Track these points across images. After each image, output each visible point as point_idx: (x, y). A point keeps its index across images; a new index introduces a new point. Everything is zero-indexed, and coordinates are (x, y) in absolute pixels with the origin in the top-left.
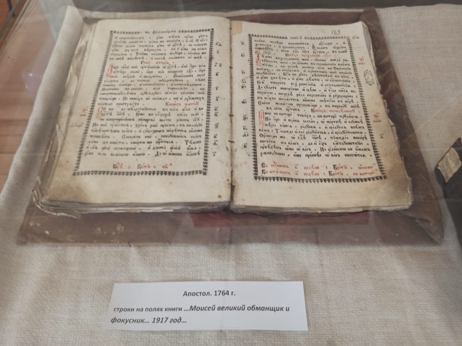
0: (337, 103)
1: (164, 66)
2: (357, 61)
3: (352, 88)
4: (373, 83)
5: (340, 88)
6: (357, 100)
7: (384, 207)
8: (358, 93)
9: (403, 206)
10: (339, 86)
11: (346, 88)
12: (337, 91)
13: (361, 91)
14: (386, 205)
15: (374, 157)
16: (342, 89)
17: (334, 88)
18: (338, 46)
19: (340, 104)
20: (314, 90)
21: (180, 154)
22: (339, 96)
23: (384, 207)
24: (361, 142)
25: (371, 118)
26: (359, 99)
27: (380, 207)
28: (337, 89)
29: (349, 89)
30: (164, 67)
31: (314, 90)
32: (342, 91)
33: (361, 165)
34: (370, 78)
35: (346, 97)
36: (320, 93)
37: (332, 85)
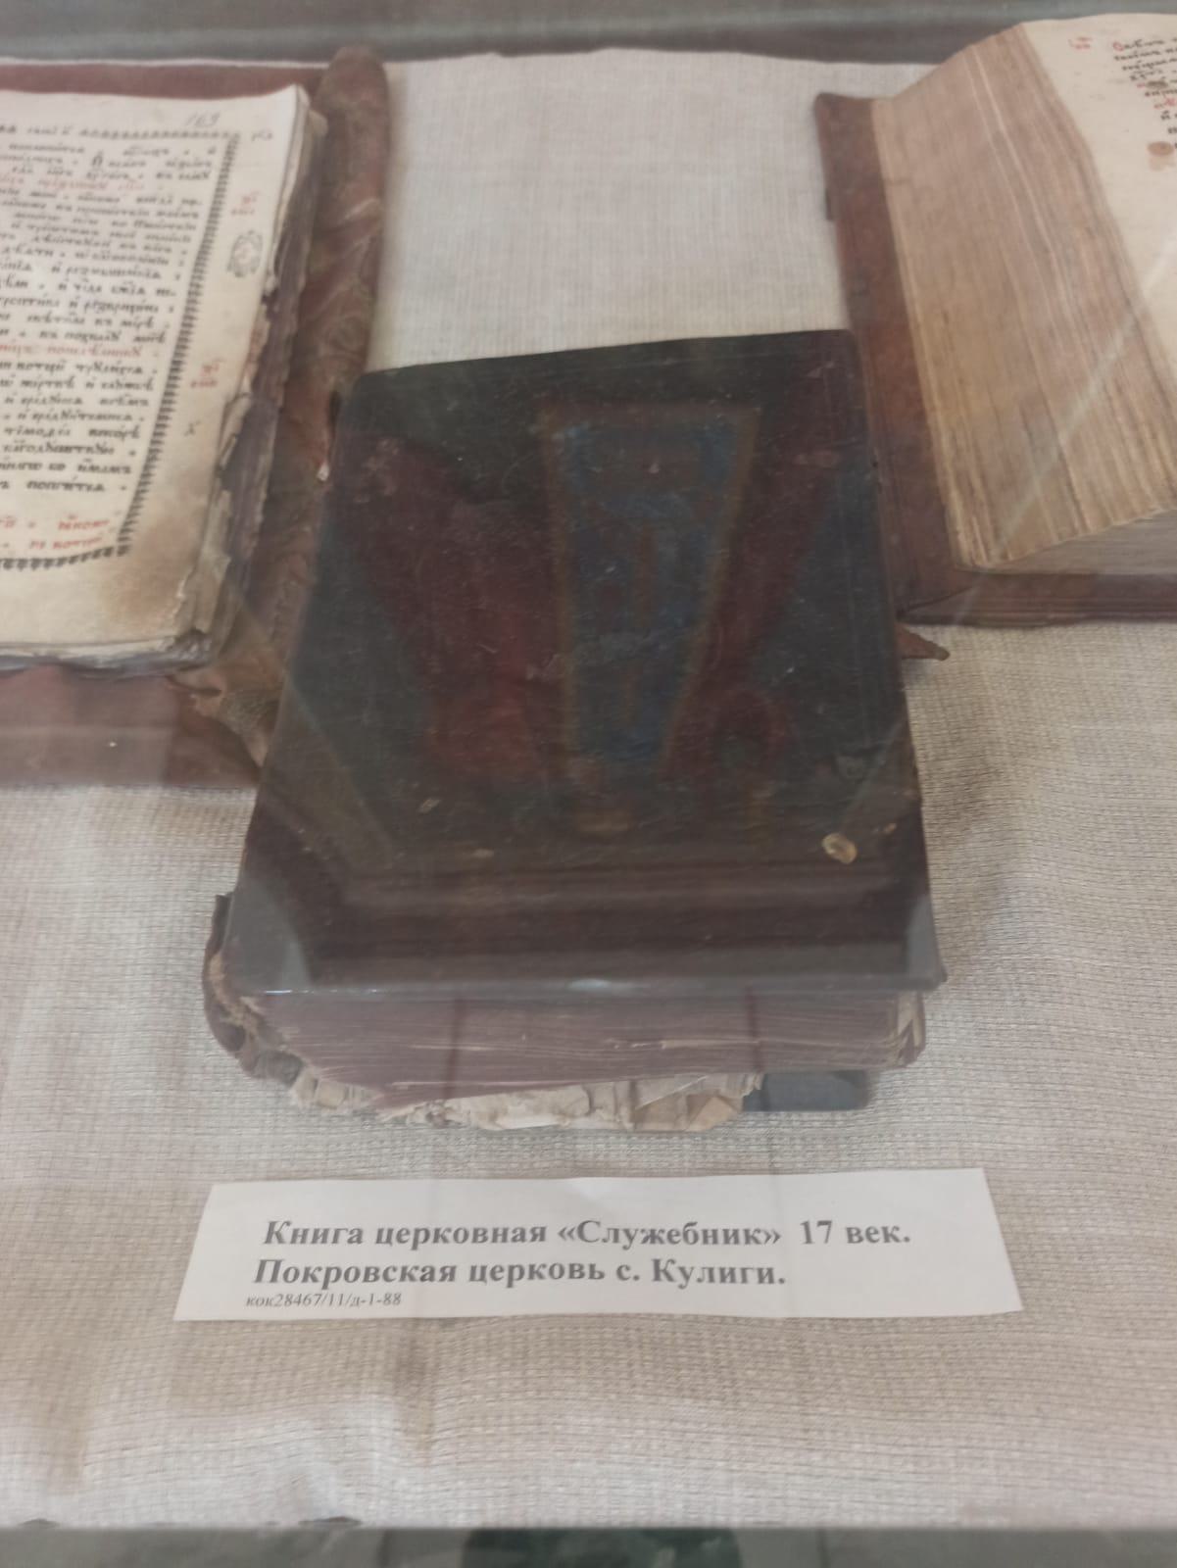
0: (89, 327)
1: (89, 379)
2: (232, 200)
3: (165, 282)
4: (253, 270)
5: (118, 281)
6: (168, 319)
7: (80, 645)
8: (180, 300)
9: (145, 640)
10: (118, 273)
11: (139, 282)
12: (106, 290)
13: (194, 292)
14: (90, 638)
15: (129, 495)
16: (128, 286)
17: (95, 280)
18: (190, 158)
19: (102, 330)
20: (22, 284)
21: (259, 1278)
22: (105, 306)
23: (80, 645)
24: (108, 446)
25: (191, 371)
26: (175, 321)
27: (66, 645)
28: (107, 283)
29: (150, 286)
30: (90, 385)
31: (22, 284)
32: (124, 290)
33: (72, 517)
34: (252, 253)
35: (131, 308)
36: (38, 295)
37: (95, 271)
